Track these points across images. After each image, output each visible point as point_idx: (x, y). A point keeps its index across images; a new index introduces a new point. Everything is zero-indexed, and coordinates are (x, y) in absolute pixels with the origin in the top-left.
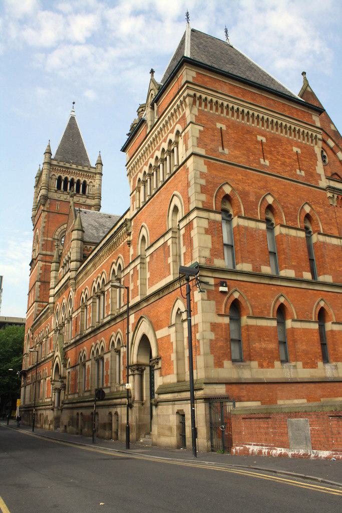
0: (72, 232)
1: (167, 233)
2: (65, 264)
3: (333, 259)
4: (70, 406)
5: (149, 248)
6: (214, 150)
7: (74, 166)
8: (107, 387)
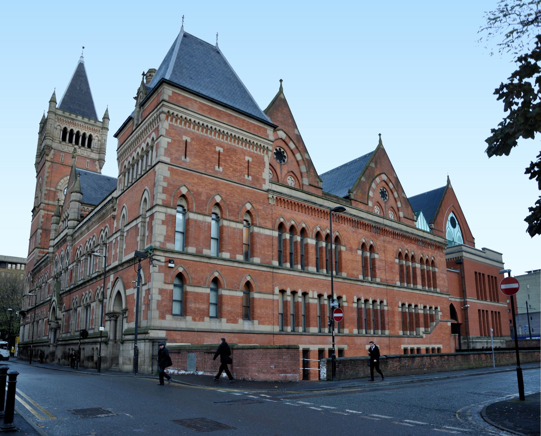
1: (138, 217)
2: (65, 220)
3: (264, 246)
4: (64, 342)
5: (127, 225)
6: (178, 159)
7: (80, 118)
8: (92, 329)
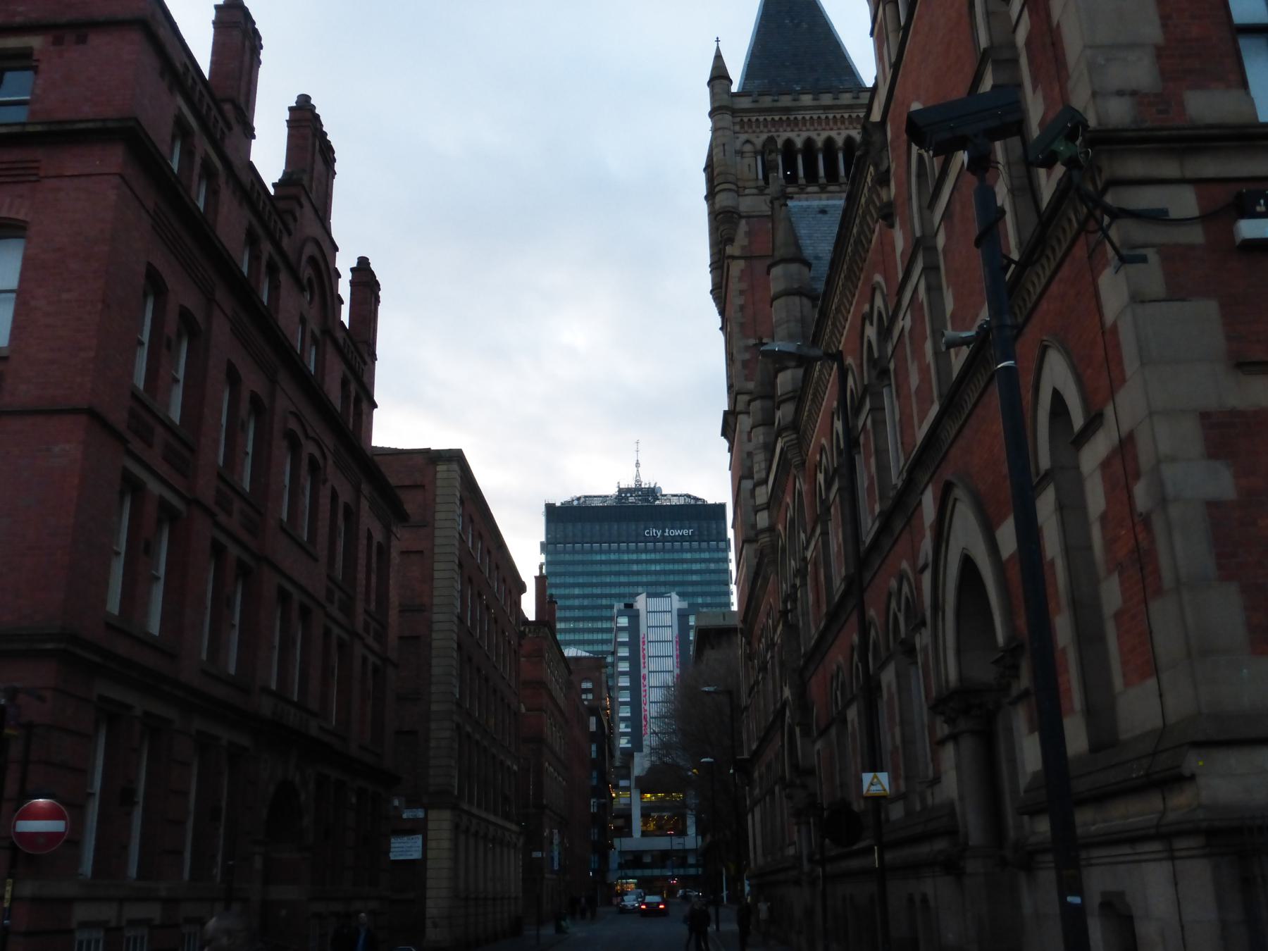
0: (768, 273)
7: (807, 100)
